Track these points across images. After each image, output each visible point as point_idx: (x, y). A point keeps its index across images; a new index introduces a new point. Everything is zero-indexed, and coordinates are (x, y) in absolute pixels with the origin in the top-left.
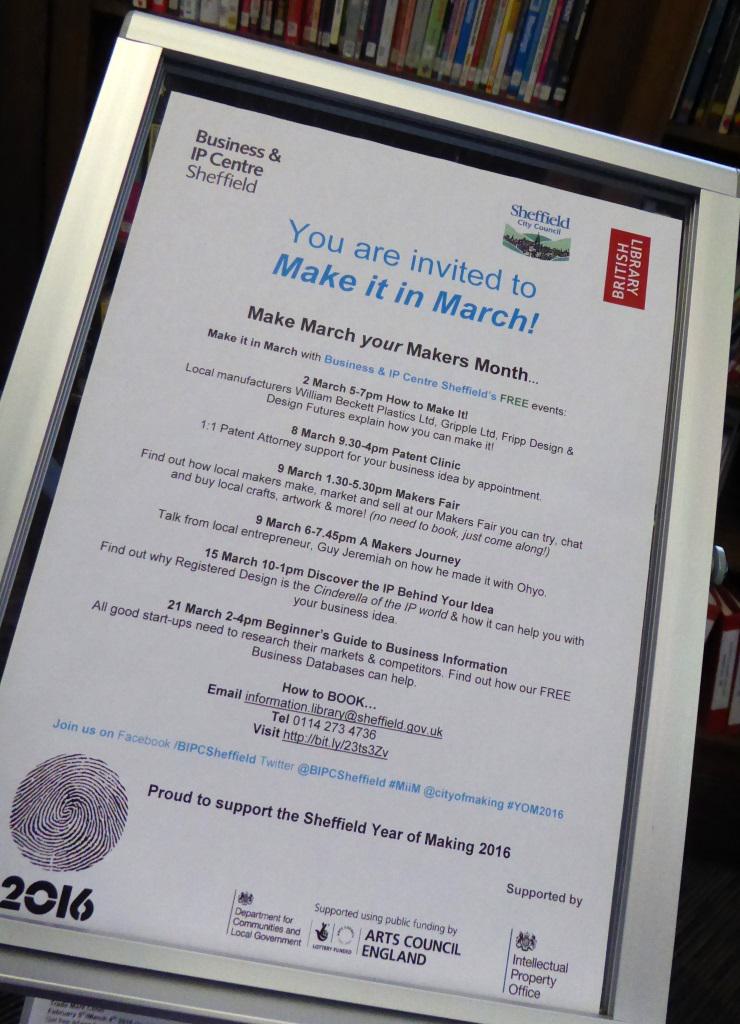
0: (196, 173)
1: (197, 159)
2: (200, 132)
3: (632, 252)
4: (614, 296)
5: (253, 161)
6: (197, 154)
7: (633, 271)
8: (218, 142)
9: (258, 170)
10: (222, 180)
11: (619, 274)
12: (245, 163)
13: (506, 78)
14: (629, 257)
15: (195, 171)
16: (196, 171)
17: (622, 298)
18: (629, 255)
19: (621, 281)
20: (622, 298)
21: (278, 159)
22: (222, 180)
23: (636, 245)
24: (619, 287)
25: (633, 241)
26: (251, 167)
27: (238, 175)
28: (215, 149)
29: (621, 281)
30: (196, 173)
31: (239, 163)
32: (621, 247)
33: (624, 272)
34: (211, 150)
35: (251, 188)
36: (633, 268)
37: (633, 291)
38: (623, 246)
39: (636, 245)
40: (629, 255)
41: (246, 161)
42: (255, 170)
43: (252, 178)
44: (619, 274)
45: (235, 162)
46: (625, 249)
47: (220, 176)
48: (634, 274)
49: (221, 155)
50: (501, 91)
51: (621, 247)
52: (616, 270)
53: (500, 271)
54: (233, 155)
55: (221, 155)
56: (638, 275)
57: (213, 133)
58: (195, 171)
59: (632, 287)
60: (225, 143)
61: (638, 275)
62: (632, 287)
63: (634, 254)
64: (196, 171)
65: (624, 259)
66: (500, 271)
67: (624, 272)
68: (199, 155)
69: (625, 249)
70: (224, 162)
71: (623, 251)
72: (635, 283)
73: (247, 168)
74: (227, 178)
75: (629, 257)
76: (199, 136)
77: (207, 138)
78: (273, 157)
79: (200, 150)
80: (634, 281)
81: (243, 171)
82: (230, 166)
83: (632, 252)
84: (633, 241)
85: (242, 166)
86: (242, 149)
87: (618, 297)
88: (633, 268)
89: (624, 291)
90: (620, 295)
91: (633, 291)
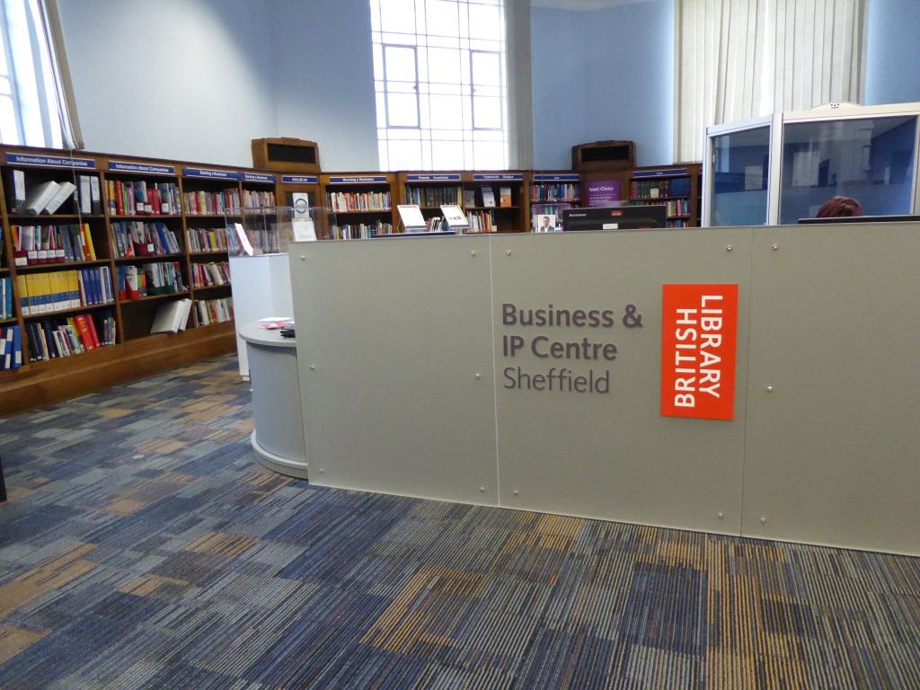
0: (516, 379)
1: (513, 354)
2: (505, 306)
3: (704, 320)
4: (677, 404)
5: (599, 337)
6: (512, 346)
7: (707, 355)
8: (538, 318)
9: (609, 351)
10: (556, 382)
11: (683, 364)
12: (586, 344)
13: (150, 193)
14: (700, 331)
15: (514, 375)
16: (515, 377)
17: (692, 405)
18: (698, 327)
19: (687, 376)
20: (692, 405)
21: (638, 323)
22: (556, 382)
23: (710, 305)
24: (685, 388)
25: (704, 298)
26: (596, 347)
27: (578, 368)
28: (535, 331)
29: (687, 376)
30: (516, 379)
31: (576, 345)
32: (682, 316)
33: (693, 359)
34: (528, 334)
35: (602, 386)
36: (709, 349)
37: (709, 390)
38: (686, 312)
39: (710, 305)
40: (698, 327)
41: (585, 340)
42: (605, 351)
43: (600, 367)
44: (683, 364)
45: (569, 346)
46: (691, 317)
47: (550, 376)
48: (711, 359)
49: (546, 339)
50: (44, 212)
51: (682, 316)
52: (678, 358)
53: (607, 372)
54: (572, 335)
55: (546, 339)
56: (717, 359)
57: (525, 305)
58: (514, 375)
59: (708, 384)
60: (546, 316)
61: (717, 359)
62: (708, 384)
63: (707, 324)
64: (515, 377)
65: (691, 335)
66: (607, 372)
67: (693, 359)
68: (514, 347)
69: (691, 317)
70: (553, 349)
71: (686, 321)
72: (714, 376)
73: (590, 352)
74: (561, 377)
75: (700, 331)
76: (505, 314)
77: (518, 315)
78: (630, 321)
79: (513, 338)
80: (710, 372)
81: (587, 357)
82: (564, 353)
83: (704, 320)
84: (704, 298)
85: (583, 350)
86: (577, 318)
87: (684, 404)
88: (709, 349)
89: (696, 394)
90: (689, 401)
91: (709, 390)
